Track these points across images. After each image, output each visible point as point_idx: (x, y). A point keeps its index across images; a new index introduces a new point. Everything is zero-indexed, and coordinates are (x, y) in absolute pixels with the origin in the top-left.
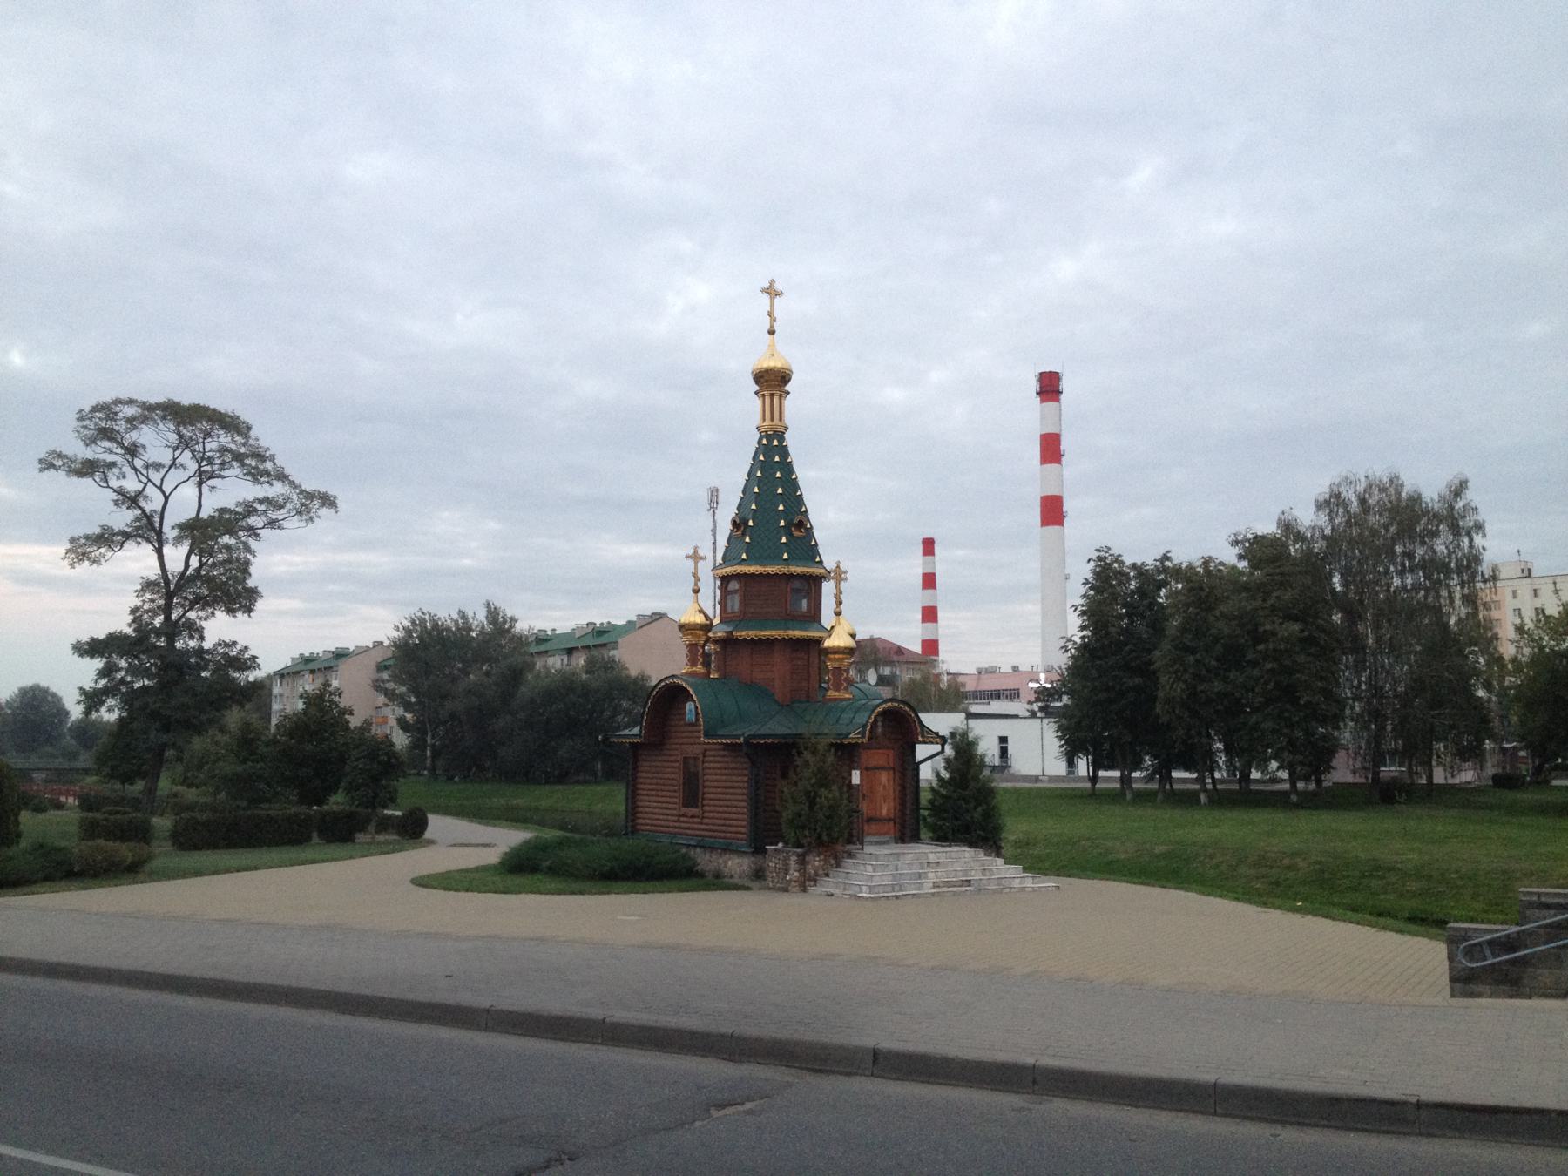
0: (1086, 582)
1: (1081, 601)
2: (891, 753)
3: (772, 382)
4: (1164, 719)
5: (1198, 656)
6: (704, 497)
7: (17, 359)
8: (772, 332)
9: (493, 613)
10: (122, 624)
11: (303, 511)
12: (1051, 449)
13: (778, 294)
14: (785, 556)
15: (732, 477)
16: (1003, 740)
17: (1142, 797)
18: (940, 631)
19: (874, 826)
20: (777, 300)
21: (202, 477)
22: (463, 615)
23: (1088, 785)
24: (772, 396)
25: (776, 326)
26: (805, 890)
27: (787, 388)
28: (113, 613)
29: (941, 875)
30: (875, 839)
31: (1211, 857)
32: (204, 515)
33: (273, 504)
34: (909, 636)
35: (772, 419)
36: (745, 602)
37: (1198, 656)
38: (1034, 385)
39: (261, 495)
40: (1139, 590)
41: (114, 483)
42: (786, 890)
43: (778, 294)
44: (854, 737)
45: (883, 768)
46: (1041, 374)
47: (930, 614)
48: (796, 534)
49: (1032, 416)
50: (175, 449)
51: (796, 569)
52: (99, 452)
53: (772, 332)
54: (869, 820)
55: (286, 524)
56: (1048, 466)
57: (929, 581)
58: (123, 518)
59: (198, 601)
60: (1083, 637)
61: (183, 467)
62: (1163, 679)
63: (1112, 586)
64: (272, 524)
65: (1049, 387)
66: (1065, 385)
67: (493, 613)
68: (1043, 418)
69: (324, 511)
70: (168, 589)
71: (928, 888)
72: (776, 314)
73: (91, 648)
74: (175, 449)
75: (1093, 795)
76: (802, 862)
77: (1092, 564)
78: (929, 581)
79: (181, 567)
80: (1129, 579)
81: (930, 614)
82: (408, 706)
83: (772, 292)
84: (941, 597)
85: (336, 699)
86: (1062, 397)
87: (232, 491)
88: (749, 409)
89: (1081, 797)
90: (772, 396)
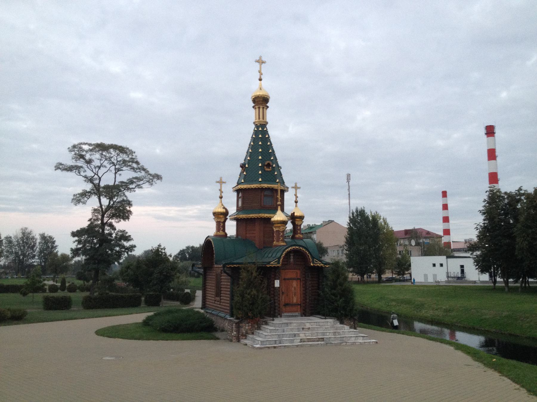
0: (485, 201)
1: (483, 209)
2: (299, 272)
4: (519, 257)
5: (533, 230)
7: (158, 151)
8: (260, 80)
10: (85, 224)
11: (150, 182)
12: (492, 155)
13: (263, 62)
14: (260, 180)
15: (240, 146)
16: (462, 266)
17: (501, 290)
18: (450, 225)
19: (288, 308)
20: (263, 65)
21: (117, 170)
23: (492, 285)
24: (259, 108)
26: (239, 341)
27: (268, 105)
29: (308, 335)
30: (285, 314)
31: (528, 318)
32: (117, 183)
33: (139, 179)
34: (437, 228)
35: (259, 118)
36: (243, 203)
37: (533, 230)
38: (484, 131)
39: (134, 176)
40: (508, 203)
41: (82, 173)
42: (231, 341)
43: (263, 62)
44: (273, 264)
45: (294, 279)
46: (487, 126)
47: (446, 220)
48: (267, 169)
49: (484, 143)
50: (101, 160)
51: (265, 186)
52: (80, 163)
54: (286, 305)
55: (143, 186)
56: (490, 161)
57: (445, 207)
58: (88, 187)
59: (112, 216)
60: (484, 223)
61: (105, 167)
62: (518, 240)
63: (496, 202)
64: (139, 186)
65: (490, 131)
66: (497, 130)
68: (488, 142)
69: (159, 181)
70: (101, 211)
71: (297, 342)
73: (74, 234)
74: (101, 160)
75: (494, 289)
76: (238, 327)
77: (488, 193)
78: (445, 207)
79: (107, 204)
80: (504, 199)
81: (446, 220)
83: (261, 62)
84: (449, 213)
85: (163, 251)
86: (496, 135)
87: (126, 175)
88: (251, 115)
89: (489, 290)
90: (263, 108)
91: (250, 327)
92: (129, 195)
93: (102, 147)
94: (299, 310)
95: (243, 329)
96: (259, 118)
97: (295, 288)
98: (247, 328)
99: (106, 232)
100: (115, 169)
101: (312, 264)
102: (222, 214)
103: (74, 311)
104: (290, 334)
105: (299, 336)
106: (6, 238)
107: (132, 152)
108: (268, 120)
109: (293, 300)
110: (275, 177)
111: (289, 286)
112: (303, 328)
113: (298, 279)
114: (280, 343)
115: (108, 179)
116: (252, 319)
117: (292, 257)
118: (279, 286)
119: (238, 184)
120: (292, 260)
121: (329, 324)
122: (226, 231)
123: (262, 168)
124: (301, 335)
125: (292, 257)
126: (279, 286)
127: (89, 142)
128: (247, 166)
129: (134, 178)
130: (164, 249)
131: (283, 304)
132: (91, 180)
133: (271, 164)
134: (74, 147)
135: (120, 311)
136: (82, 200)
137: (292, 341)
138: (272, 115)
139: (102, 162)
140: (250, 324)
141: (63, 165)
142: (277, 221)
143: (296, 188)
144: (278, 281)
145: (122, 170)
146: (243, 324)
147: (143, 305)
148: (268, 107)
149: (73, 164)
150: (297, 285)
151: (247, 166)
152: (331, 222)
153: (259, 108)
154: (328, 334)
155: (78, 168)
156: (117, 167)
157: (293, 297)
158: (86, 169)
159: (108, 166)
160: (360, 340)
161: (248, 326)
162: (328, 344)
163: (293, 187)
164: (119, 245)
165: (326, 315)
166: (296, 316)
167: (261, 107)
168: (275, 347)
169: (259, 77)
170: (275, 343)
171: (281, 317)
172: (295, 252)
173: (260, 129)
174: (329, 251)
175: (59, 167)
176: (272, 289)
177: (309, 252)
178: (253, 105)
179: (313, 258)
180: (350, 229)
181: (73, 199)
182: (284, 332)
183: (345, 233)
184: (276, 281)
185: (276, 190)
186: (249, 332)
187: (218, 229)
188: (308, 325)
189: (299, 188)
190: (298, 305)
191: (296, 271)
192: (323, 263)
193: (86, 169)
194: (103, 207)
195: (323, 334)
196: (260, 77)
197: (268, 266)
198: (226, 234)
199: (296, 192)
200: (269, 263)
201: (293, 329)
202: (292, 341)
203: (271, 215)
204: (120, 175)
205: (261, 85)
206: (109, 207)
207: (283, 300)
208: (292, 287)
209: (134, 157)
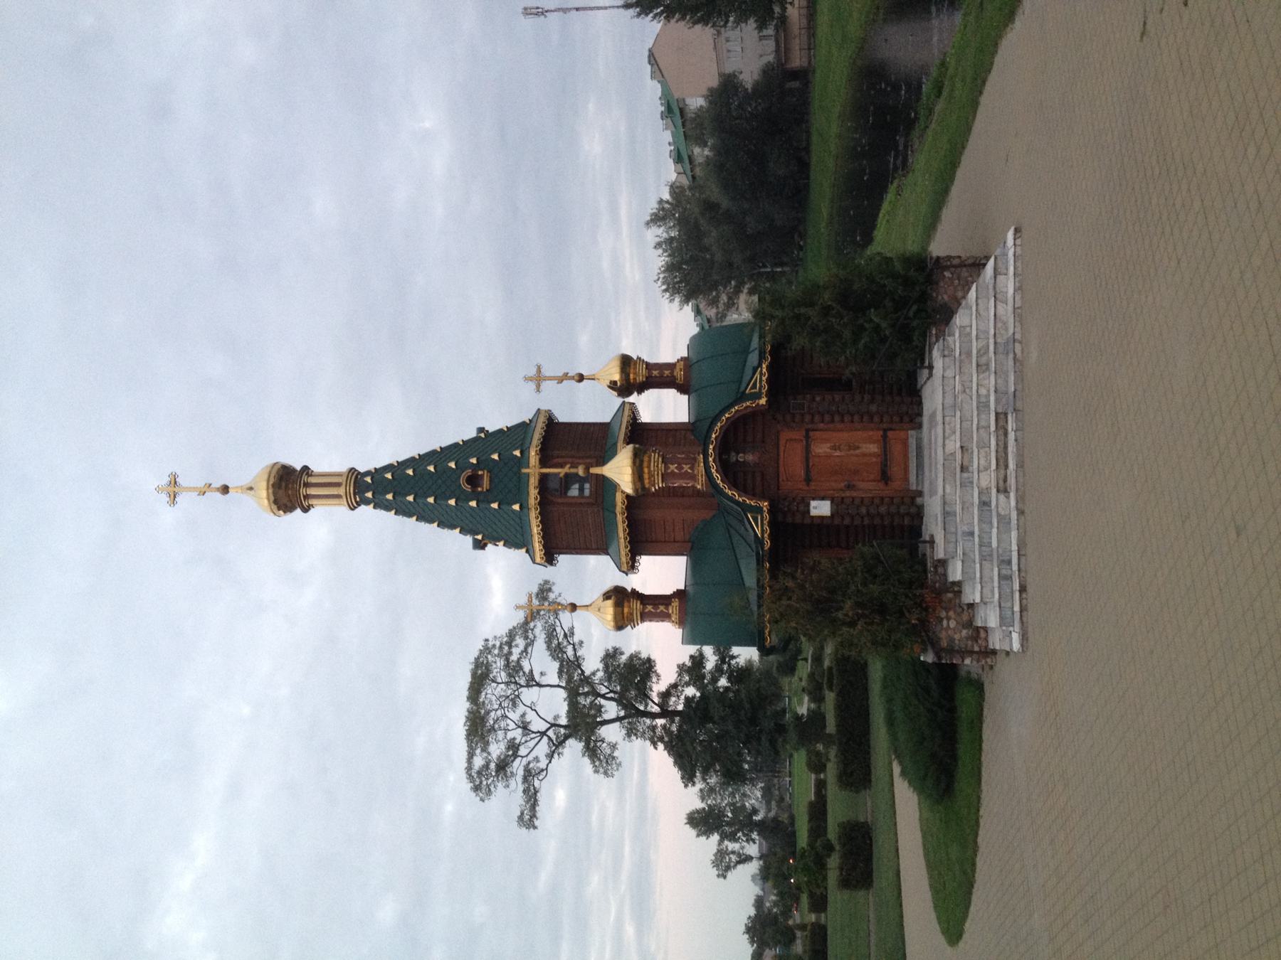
2: (786, 435)
3: (290, 488)
6: (531, 21)
9: (656, 219)
13: (174, 482)
14: (516, 507)
19: (895, 470)
21: (531, 682)
22: (658, 245)
24: (307, 497)
25: (218, 484)
28: (661, 761)
30: (912, 478)
33: (551, 634)
35: (338, 496)
41: (542, 765)
43: (174, 482)
45: (807, 449)
48: (486, 483)
51: (533, 493)
52: (518, 767)
53: (225, 489)
54: (885, 477)
59: (644, 695)
61: (523, 715)
67: (656, 219)
70: (632, 715)
72: (201, 484)
79: (614, 704)
82: (738, 291)
87: (542, 663)
88: (324, 523)
90: (307, 485)
91: (951, 613)
92: (592, 663)
93: (478, 728)
94: (902, 434)
95: (957, 637)
96: (338, 496)
97: (834, 448)
98: (952, 624)
99: (680, 708)
100: (528, 686)
101: (763, 401)
102: (618, 605)
104: (980, 520)
105: (989, 489)
106: (703, 799)
107: (487, 649)
108: (343, 468)
109: (870, 455)
110: (507, 460)
111: (826, 467)
112: (963, 469)
113: (807, 437)
114: (1009, 562)
115: (551, 704)
116: (926, 609)
117: (741, 457)
118: (828, 503)
119: (517, 540)
120: (750, 457)
121: (949, 373)
122: (669, 592)
123: (483, 499)
124: (984, 484)
125: (741, 457)
126: (828, 503)
127: (465, 755)
128: (479, 537)
129: (549, 648)
130: (721, 855)
131: (881, 485)
132: (557, 745)
133: (469, 472)
134: (477, 789)
136: (608, 751)
137: (1004, 521)
138: (327, 457)
139: (512, 726)
140: (943, 614)
141: (522, 813)
142: (634, 482)
143: (538, 379)
144: (813, 503)
145: (531, 671)
146: (943, 635)
148: (305, 468)
149: (521, 788)
150: (827, 440)
151: (479, 537)
152: (650, 50)
153: (307, 497)
154: (983, 391)
155: (529, 774)
156: (523, 682)
157: (864, 455)
158: (530, 758)
159: (521, 709)
160: (1009, 285)
161: (948, 619)
162: (1019, 405)
164: (715, 680)
165: (920, 359)
166: (919, 448)
167: (303, 491)
168: (1023, 589)
169: (218, 495)
170: (1009, 578)
171: (920, 494)
172: (725, 447)
173: (369, 495)
174: (729, 69)
175: (529, 818)
176: (837, 521)
177: (722, 412)
178: (298, 511)
179: (742, 397)
180: (669, 13)
181: (606, 773)
182: (972, 534)
183: (681, 29)
184: (814, 512)
185: (543, 479)
186: (965, 617)
187: (664, 617)
188: (954, 445)
189: (538, 390)
190: (885, 437)
191: (782, 442)
192: (760, 365)
193: (530, 758)
194: (622, 713)
195: (983, 406)
197: (767, 544)
198: (679, 594)
199: (551, 378)
200: (760, 542)
201: (963, 503)
202: (1004, 521)
203: (619, 498)
204: (542, 674)
206: (621, 700)
207: (871, 485)
208: (829, 457)
209: (498, 644)
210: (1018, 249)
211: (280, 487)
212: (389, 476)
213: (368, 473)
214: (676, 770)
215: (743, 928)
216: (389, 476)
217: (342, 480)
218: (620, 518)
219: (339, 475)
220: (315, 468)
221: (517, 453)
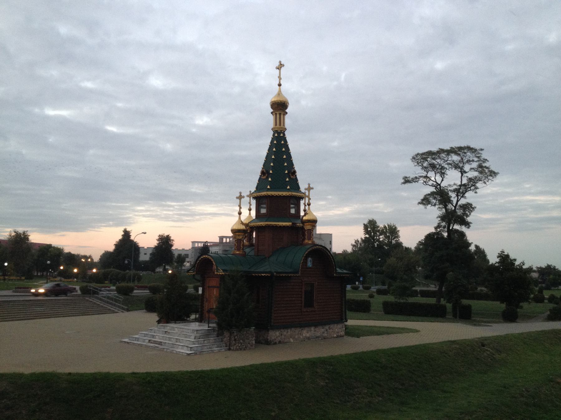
14: (269, 187)
24: (276, 114)
27: (287, 111)
35: (276, 125)
45: (214, 287)
88: (269, 120)
90: (280, 114)
103: (475, 320)
110: (286, 184)
119: (259, 188)
135: (400, 317)
147: (450, 316)
153: (276, 114)
163: (244, 197)
167: (278, 113)
178: (272, 110)
196: (280, 82)
205: (280, 91)
210: (165, 350)
211: (278, 105)
212: (283, 142)
213: (284, 135)
214: (423, 238)
215: (550, 264)
216: (283, 142)
217: (282, 126)
218: (267, 223)
219: (284, 125)
220: (286, 116)
221: (288, 187)
